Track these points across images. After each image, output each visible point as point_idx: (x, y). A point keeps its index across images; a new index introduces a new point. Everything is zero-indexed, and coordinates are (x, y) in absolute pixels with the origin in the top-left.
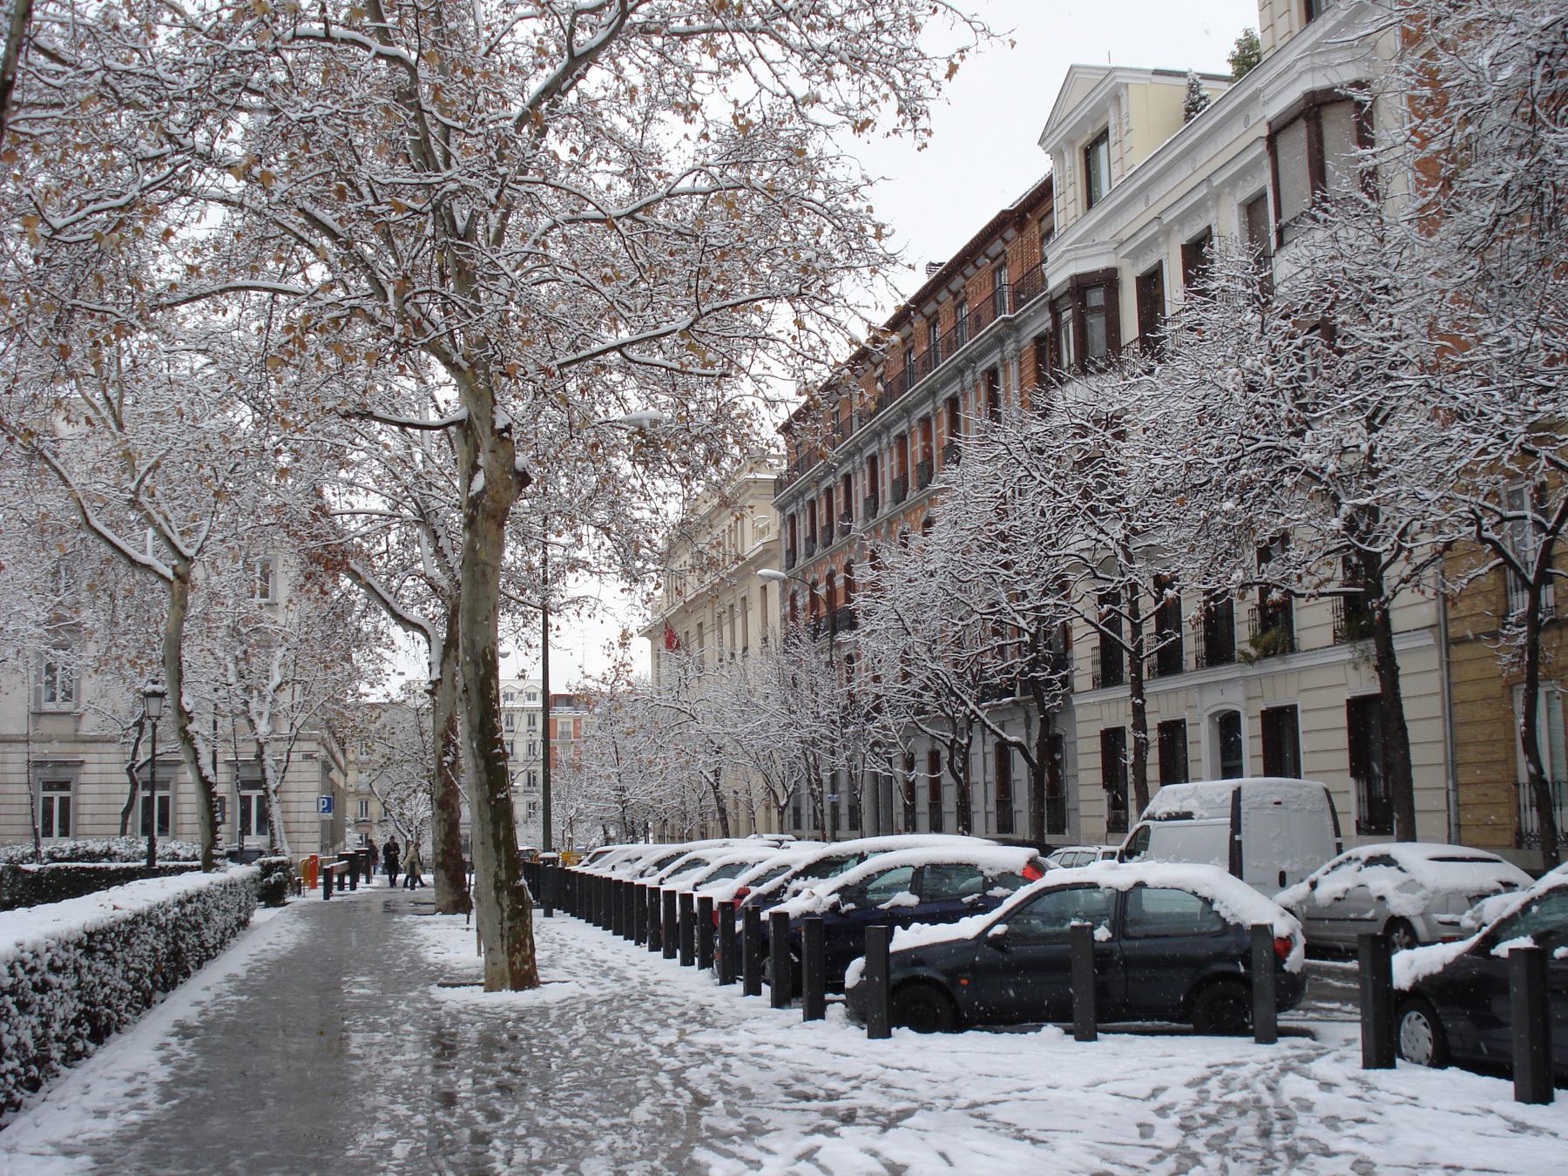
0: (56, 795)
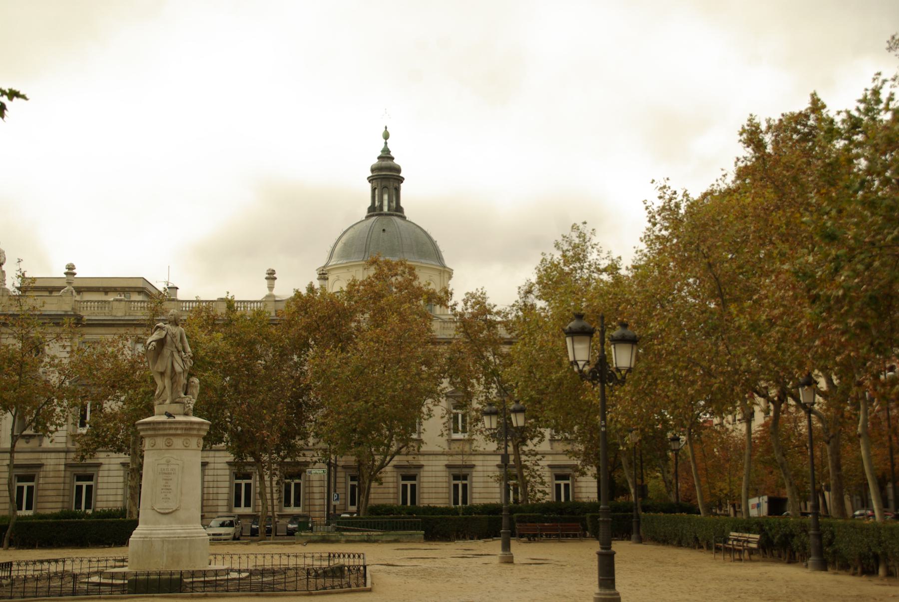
0: (409, 483)
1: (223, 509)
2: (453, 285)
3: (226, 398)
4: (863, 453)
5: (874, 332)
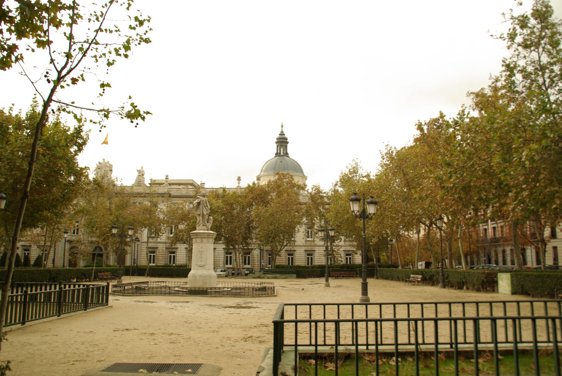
0: (290, 257)
1: (221, 265)
2: (307, 182)
3: (222, 224)
4: (460, 245)
5: (464, 200)
